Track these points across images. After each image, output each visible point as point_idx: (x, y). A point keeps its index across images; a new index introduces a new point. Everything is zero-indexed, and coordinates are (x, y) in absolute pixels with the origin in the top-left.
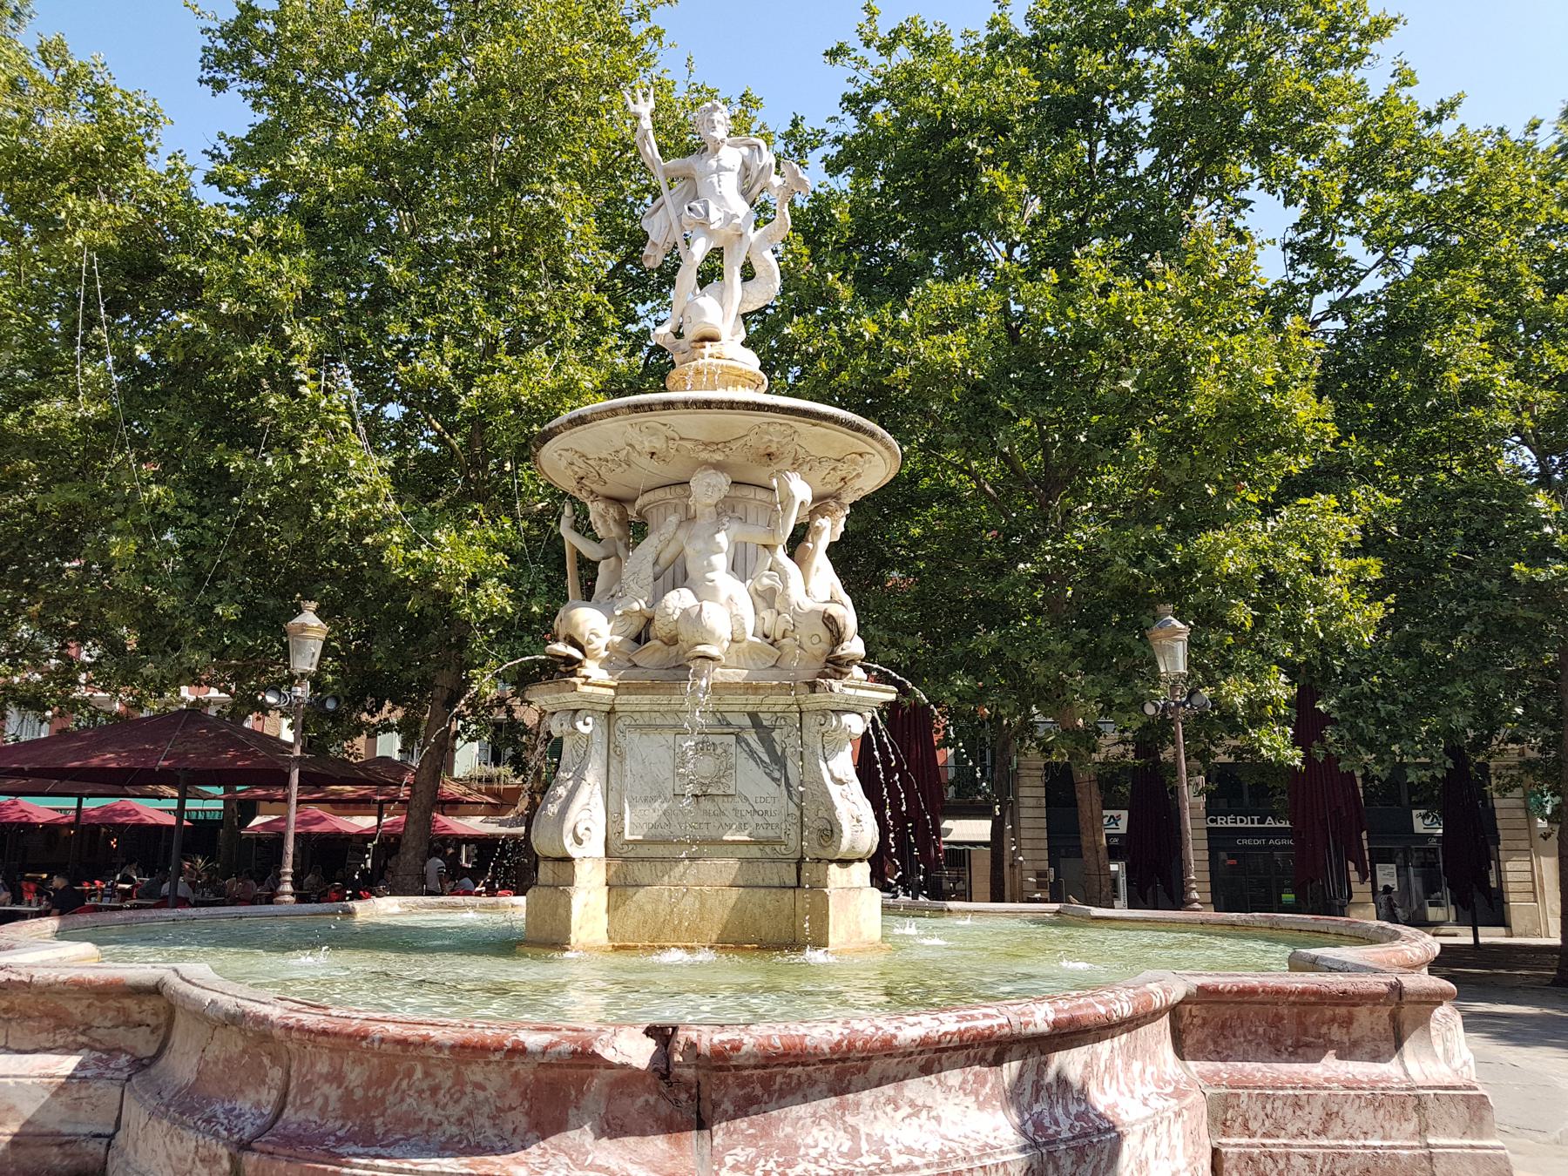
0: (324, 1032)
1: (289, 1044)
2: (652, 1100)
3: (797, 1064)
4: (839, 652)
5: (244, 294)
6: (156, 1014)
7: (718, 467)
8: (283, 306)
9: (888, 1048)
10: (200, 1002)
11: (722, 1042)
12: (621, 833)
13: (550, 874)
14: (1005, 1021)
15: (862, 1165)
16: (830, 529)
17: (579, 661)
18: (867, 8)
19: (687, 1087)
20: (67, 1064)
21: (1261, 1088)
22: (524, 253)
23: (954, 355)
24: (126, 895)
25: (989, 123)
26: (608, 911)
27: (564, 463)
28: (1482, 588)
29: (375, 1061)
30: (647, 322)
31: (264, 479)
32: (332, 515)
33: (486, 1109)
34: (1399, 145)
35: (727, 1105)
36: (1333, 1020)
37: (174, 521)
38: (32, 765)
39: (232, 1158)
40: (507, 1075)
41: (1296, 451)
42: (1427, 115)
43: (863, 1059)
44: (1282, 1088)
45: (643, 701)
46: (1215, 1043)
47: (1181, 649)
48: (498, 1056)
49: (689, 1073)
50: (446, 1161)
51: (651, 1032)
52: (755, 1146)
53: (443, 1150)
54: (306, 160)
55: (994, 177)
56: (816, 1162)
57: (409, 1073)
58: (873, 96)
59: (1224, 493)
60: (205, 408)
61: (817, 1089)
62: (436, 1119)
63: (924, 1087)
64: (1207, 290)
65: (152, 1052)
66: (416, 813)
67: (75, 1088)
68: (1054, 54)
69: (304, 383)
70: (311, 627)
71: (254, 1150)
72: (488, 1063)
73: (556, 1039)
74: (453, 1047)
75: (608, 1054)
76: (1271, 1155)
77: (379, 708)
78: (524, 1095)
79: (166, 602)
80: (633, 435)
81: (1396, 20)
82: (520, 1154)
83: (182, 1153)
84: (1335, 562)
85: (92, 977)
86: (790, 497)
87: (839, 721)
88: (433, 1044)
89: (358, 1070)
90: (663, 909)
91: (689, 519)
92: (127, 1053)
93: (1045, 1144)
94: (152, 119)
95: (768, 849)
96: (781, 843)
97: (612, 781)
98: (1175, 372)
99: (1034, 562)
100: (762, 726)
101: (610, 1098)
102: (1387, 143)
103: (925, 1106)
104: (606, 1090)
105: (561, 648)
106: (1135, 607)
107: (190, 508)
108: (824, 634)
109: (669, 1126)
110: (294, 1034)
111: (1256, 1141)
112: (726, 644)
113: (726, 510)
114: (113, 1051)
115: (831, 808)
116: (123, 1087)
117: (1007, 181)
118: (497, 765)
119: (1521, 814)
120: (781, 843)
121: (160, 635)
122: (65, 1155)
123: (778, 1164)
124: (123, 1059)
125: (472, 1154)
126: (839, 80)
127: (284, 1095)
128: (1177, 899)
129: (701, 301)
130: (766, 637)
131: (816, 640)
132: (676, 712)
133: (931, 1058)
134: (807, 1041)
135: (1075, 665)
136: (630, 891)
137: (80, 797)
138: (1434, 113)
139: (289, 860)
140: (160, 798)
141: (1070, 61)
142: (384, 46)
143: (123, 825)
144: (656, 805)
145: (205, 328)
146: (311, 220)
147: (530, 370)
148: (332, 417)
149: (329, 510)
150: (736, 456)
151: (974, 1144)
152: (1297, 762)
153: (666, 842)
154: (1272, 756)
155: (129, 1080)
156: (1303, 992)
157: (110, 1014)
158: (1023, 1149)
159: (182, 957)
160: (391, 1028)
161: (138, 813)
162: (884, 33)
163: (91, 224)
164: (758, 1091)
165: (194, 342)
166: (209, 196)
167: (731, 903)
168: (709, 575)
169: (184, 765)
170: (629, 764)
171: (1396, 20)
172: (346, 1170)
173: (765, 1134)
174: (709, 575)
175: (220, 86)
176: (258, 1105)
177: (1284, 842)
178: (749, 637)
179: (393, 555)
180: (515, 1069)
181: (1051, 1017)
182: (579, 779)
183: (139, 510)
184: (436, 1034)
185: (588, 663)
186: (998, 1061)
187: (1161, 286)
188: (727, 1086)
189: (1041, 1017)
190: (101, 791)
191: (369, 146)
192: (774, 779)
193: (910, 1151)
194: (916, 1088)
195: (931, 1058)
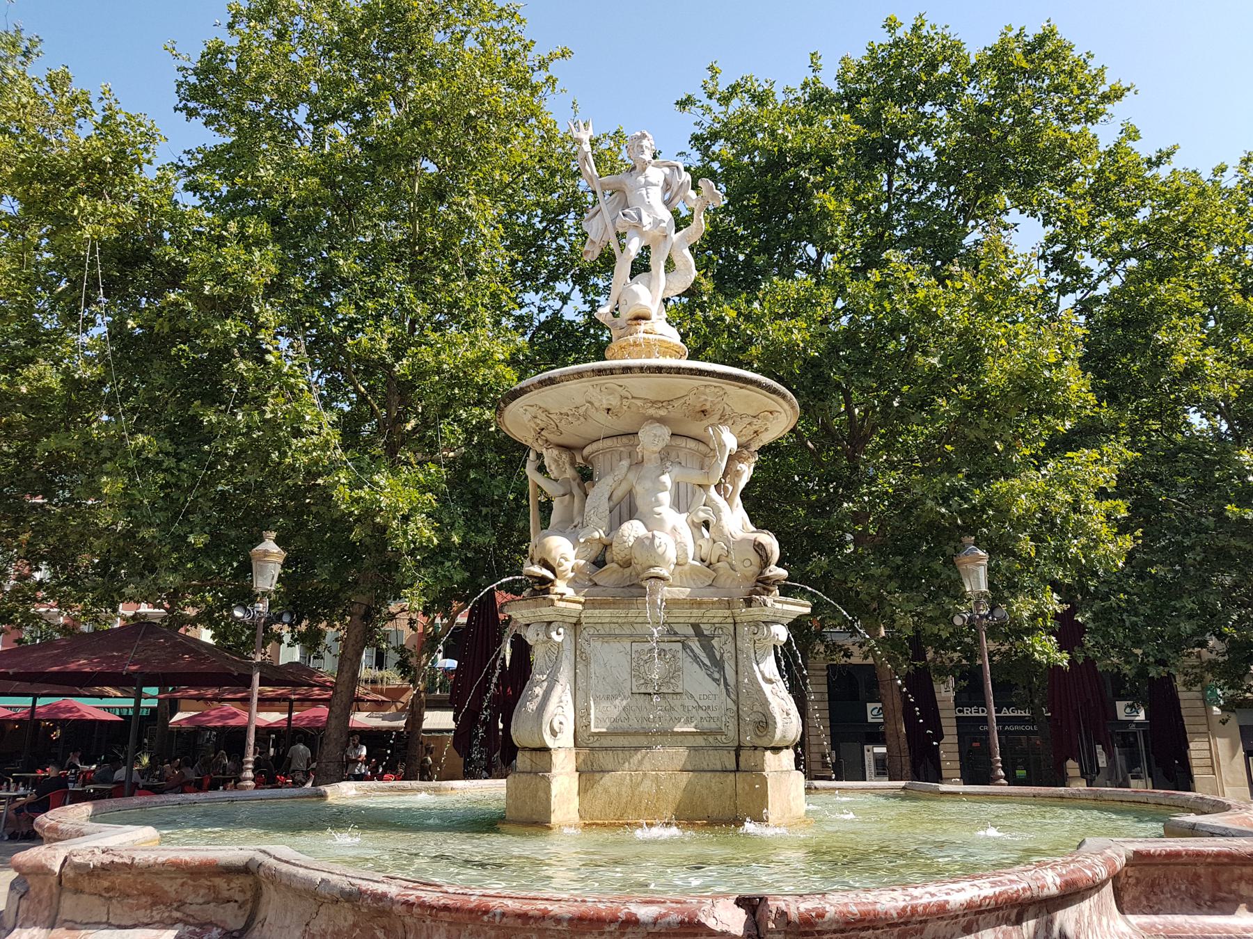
0: (446, 908)
1: (408, 920)
3: (868, 928)
4: (768, 574)
5: (223, 279)
6: (243, 891)
7: (661, 421)
8: (256, 289)
10: (311, 881)
12: (588, 726)
13: (528, 762)
16: (746, 471)
17: (551, 581)
18: (711, 68)
22: (442, 252)
23: (796, 336)
25: (818, 157)
28: (1200, 524)
30: (532, 308)
31: (232, 432)
32: (288, 460)
34: (1129, 183)
36: (1241, 878)
37: (157, 466)
38: (15, 670)
41: (1063, 415)
42: (1149, 161)
43: (921, 922)
45: (605, 614)
46: (1148, 899)
47: (982, 572)
48: (613, 927)
51: (740, 902)
54: (272, 172)
55: (825, 199)
58: (715, 136)
59: (1010, 448)
60: (179, 372)
64: (996, 288)
65: (240, 924)
66: (337, 710)
68: (865, 106)
69: (270, 352)
72: (601, 934)
73: (663, 911)
74: (571, 920)
75: (711, 923)
80: (594, 394)
81: (1129, 89)
84: (1091, 503)
85: (188, 859)
86: (722, 445)
87: (769, 630)
88: (552, 917)
92: (218, 927)
94: (150, 137)
95: (711, 739)
96: (722, 733)
97: (579, 682)
98: (969, 353)
102: (1121, 178)
106: (945, 539)
107: (167, 454)
108: (755, 558)
110: (416, 910)
112: (672, 567)
113: (666, 457)
114: (205, 925)
115: (765, 703)
117: (834, 202)
118: (380, 669)
119: (1200, 704)
120: (722, 733)
126: (690, 123)
128: (988, 779)
129: (635, 287)
130: (703, 561)
132: (632, 624)
134: (878, 907)
135: (893, 585)
136: (597, 776)
138: (1154, 159)
139: (251, 750)
141: (877, 112)
142: (334, 86)
143: (67, 720)
144: (617, 702)
145: (190, 306)
146: (275, 220)
147: (452, 344)
148: (292, 380)
149: (286, 456)
150: (676, 411)
153: (625, 733)
156: (1218, 855)
157: (202, 892)
161: (79, 711)
162: (723, 88)
163: (96, 221)
165: (179, 318)
166: (189, 200)
167: (683, 785)
168: (657, 509)
170: (593, 667)
171: (1129, 89)
174: (657, 509)
175: (191, 113)
177: (1017, 728)
178: (690, 560)
179: (342, 494)
181: (1058, 881)
182: (553, 682)
184: (554, 908)
185: (558, 582)
186: (1019, 921)
187: (958, 285)
189: (1051, 881)
190: (56, 692)
191: (324, 162)
192: (714, 680)
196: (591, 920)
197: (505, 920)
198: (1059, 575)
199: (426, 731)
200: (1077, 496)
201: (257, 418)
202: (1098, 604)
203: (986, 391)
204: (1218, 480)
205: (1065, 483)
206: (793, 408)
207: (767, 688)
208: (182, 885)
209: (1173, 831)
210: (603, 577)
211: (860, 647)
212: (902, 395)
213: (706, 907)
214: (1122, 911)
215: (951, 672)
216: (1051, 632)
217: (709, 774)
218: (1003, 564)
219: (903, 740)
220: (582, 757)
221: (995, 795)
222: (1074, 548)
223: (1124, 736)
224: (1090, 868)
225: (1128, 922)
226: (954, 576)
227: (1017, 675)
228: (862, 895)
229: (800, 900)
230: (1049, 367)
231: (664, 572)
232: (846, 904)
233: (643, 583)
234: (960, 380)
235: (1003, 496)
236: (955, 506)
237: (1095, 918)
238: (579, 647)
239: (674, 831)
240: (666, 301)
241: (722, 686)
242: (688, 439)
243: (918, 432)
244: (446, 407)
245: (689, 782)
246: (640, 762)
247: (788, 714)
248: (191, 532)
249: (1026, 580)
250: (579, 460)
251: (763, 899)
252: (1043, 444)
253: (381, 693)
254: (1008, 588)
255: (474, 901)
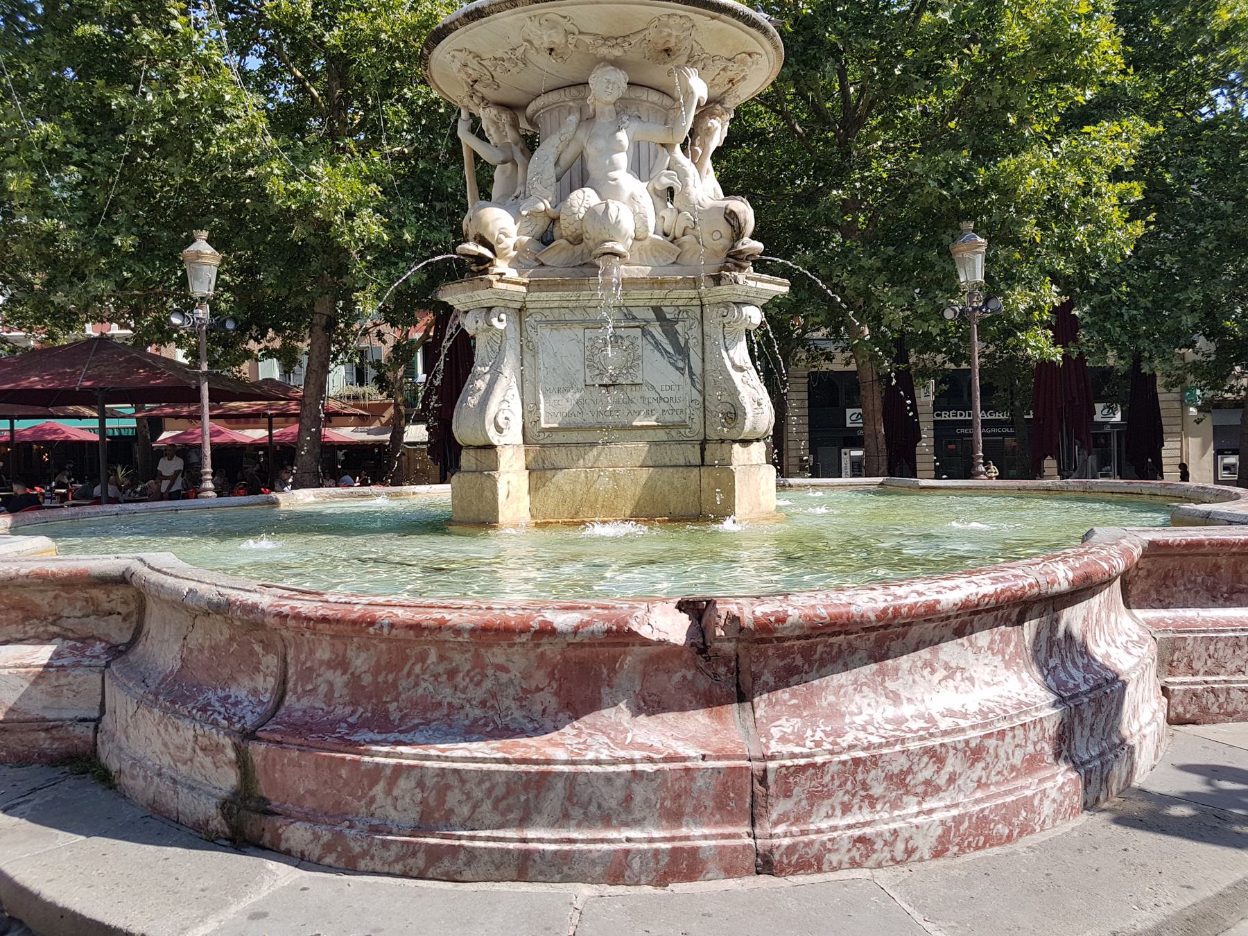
0: (325, 619)
1: (284, 632)
2: (690, 675)
3: (839, 633)
4: (740, 247)
6: (125, 603)
7: (616, 63)
9: (930, 614)
10: (178, 592)
11: (765, 614)
12: (537, 421)
13: (473, 461)
14: (1034, 582)
15: (911, 731)
16: (718, 131)
17: (490, 260)
19: (726, 660)
20: (42, 654)
21: (1204, 631)
24: (64, 497)
26: (529, 493)
27: (457, 64)
29: (383, 646)
31: (145, 117)
33: (511, 691)
35: (768, 677)
39: (236, 747)
40: (532, 655)
43: (904, 625)
44: (1223, 631)
45: (552, 298)
46: (1158, 592)
47: (979, 261)
48: (524, 638)
49: (728, 647)
50: (475, 745)
51: (683, 606)
52: (800, 716)
53: (470, 733)
56: (864, 730)
57: (423, 658)
59: (1022, 121)
61: (857, 656)
62: (456, 702)
63: (957, 649)
65: (127, 638)
67: (53, 677)
69: (176, 18)
70: (205, 263)
71: (259, 739)
72: (512, 645)
73: (586, 618)
75: (645, 631)
76: (1213, 691)
77: (264, 335)
78: (551, 675)
79: (69, 239)
80: (532, 28)
82: (554, 735)
83: (179, 741)
84: (1105, 187)
85: (54, 569)
86: (689, 93)
87: (740, 312)
88: (450, 628)
89: (363, 655)
90: (580, 490)
91: (587, 119)
92: (101, 640)
93: (1071, 697)
95: (674, 433)
96: (686, 427)
99: (844, 189)
100: (665, 319)
101: (645, 675)
103: (958, 668)
104: (640, 667)
105: (472, 247)
106: (940, 225)
107: (79, 146)
108: (725, 229)
109: (708, 701)
110: (291, 623)
111: (1199, 678)
112: (630, 242)
113: (623, 109)
115: (735, 392)
116: (103, 673)
118: (361, 385)
119: (1177, 405)
120: (686, 427)
121: (68, 271)
122: (54, 739)
123: (827, 734)
124: (99, 647)
125: (501, 737)
127: (283, 682)
128: (969, 473)
130: (666, 235)
131: (717, 236)
132: (584, 308)
133: (965, 621)
134: (853, 609)
136: (549, 474)
137: (12, 419)
140: (80, 417)
143: (53, 442)
144: (569, 395)
149: (210, 144)
150: (632, 52)
151: (1008, 703)
152: (1059, 357)
153: (579, 429)
154: (1037, 354)
155: (108, 665)
157: (79, 604)
158: (1054, 705)
159: (144, 547)
160: (400, 612)
164: (799, 661)
167: (642, 481)
168: (613, 174)
169: (101, 385)
172: (366, 759)
173: (808, 703)
174: (613, 174)
176: (255, 692)
177: (993, 430)
178: (651, 234)
179: (275, 186)
180: (541, 649)
181: (1071, 575)
183: (30, 146)
184: (453, 618)
185: (498, 262)
186: (1020, 621)
188: (767, 658)
189: (1062, 575)
192: (678, 369)
193: (951, 713)
194: (950, 651)
195: (965, 621)
196: (497, 630)
197: (394, 631)
198: (1060, 265)
199: (408, 443)
200: (1090, 178)
201: (169, 98)
202: (1096, 299)
203: (1002, 51)
204: (1243, 161)
205: (1077, 161)
206: (776, 48)
207: (736, 376)
208: (56, 597)
209: (1180, 520)
210: (549, 256)
211: (843, 351)
212: (905, 60)
213: (639, 613)
214: (1128, 606)
215: (933, 374)
216: (1046, 325)
217: (671, 470)
218: (1002, 253)
219: (881, 440)
220: (532, 454)
221: (978, 488)
222: (1081, 234)
223: (1097, 439)
224: (1106, 560)
225: (1134, 617)
226: (948, 268)
227: (1006, 376)
228: (833, 595)
229: (757, 602)
230: (1076, 19)
231: (619, 247)
232: (813, 606)
233: (597, 261)
234: (974, 40)
235: (1010, 175)
236: (956, 188)
237: (1103, 615)
238: (525, 334)
239: (629, 528)
241: (687, 375)
242: (648, 91)
243: (922, 104)
244: (387, 84)
245: (650, 478)
246: (597, 459)
247: (759, 404)
248: (117, 233)
249: (1025, 271)
250: (524, 125)
251: (711, 603)
252: (1057, 119)
253: (364, 408)
254: (1005, 279)
255: (358, 611)
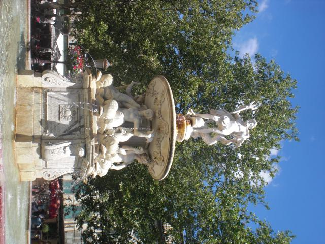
86: (148, 134)
150: (158, 122)
240: (247, 15)
